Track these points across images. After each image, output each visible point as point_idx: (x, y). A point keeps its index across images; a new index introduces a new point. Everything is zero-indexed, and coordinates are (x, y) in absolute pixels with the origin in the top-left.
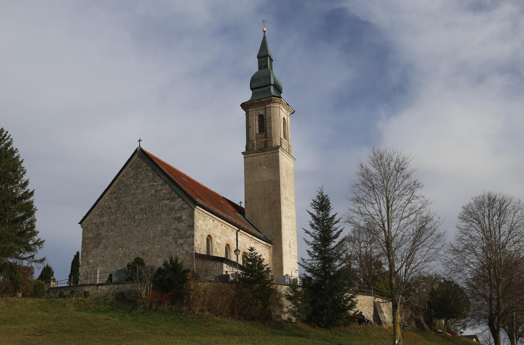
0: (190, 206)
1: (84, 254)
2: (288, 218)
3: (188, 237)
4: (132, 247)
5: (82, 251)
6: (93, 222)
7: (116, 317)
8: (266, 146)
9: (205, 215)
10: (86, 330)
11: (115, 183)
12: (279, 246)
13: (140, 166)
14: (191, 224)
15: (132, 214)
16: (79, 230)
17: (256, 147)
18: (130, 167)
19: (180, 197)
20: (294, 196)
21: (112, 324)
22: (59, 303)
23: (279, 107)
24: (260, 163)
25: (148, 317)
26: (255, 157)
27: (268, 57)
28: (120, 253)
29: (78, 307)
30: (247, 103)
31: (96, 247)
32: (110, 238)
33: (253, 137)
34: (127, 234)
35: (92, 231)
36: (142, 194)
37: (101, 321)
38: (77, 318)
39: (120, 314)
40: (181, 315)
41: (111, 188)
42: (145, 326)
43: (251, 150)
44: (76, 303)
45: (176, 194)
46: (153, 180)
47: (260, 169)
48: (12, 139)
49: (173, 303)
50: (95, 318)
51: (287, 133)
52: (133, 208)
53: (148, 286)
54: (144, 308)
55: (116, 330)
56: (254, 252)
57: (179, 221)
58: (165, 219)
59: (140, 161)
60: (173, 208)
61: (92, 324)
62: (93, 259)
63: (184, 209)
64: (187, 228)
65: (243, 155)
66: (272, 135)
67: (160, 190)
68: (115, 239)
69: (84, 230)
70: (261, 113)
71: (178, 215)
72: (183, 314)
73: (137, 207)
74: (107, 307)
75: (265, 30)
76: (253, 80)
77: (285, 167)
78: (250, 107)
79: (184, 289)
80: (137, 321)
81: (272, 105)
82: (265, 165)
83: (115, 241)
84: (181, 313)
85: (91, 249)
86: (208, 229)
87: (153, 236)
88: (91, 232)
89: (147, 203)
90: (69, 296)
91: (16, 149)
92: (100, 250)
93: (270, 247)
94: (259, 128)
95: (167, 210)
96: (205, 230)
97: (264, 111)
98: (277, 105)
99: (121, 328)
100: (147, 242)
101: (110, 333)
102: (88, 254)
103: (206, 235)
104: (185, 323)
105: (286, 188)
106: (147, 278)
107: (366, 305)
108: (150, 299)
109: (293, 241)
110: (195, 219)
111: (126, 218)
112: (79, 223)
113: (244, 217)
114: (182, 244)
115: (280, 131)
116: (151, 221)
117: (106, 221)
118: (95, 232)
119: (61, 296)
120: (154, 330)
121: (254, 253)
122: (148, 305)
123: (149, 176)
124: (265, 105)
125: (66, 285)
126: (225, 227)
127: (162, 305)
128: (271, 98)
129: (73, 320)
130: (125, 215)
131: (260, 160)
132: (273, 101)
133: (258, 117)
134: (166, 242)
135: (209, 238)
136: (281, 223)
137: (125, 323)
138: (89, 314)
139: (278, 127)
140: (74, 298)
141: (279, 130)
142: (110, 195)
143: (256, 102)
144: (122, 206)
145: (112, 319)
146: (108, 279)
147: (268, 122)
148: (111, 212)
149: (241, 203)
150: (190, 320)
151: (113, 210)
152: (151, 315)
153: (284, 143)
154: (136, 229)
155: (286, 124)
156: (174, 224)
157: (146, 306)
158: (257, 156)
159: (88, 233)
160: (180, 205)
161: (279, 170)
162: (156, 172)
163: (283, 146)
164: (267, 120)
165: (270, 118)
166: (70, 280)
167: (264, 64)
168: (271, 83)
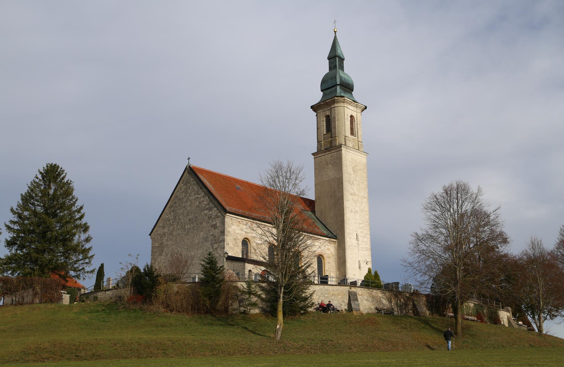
0: (222, 214)
3: (220, 242)
9: (240, 220)
11: (173, 197)
12: (343, 240)
15: (184, 225)
16: (149, 240)
17: (324, 147)
19: (216, 207)
24: (327, 162)
26: (323, 157)
31: (160, 255)
36: (190, 206)
41: (170, 203)
47: (327, 168)
48: (66, 173)
63: (218, 217)
64: (220, 234)
66: (336, 134)
70: (327, 114)
71: (214, 223)
78: (318, 109)
81: (336, 105)
91: (71, 181)
93: (335, 242)
97: (330, 111)
98: (342, 104)
100: (193, 248)
107: (338, 295)
110: (225, 225)
111: (180, 228)
113: (315, 215)
116: (196, 229)
130: (179, 226)
139: (342, 126)
141: (344, 129)
147: (333, 122)
151: (171, 222)
158: (324, 156)
160: (215, 214)
162: (199, 186)
165: (335, 117)
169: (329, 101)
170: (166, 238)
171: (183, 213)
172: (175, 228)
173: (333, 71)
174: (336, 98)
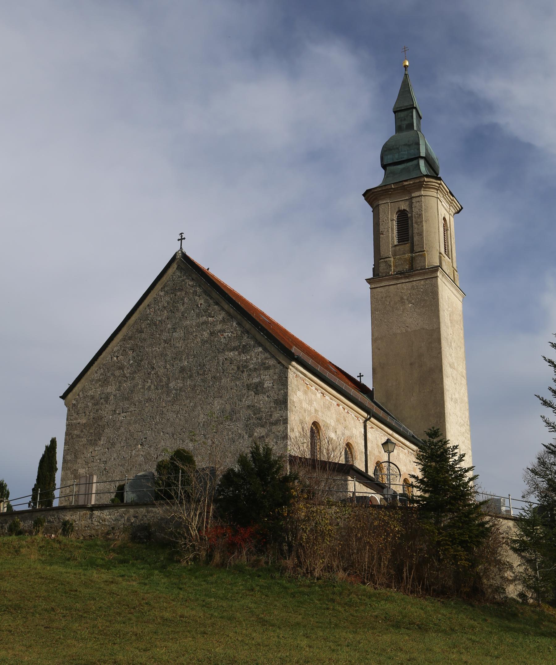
0: (280, 363)
1: (69, 458)
2: (456, 401)
3: (276, 423)
4: (163, 443)
5: (64, 450)
6: (89, 394)
7: (134, 578)
8: (412, 268)
9: (308, 381)
10: (58, 606)
11: (133, 318)
13: (181, 286)
14: (281, 397)
15: (165, 379)
16: (62, 409)
18: (162, 288)
19: (260, 344)
20: (465, 362)
21: (125, 593)
22: (6, 546)
23: (436, 196)
24: (402, 298)
25: (204, 581)
26: (391, 286)
27: (414, 111)
28: (138, 456)
29: (48, 554)
30: (376, 190)
31: (93, 443)
32: (120, 427)
33: (387, 250)
34: (153, 417)
35: (85, 413)
37: (98, 586)
38: (41, 578)
39: (142, 572)
40: (281, 577)
41: (124, 329)
42: (204, 601)
43: (384, 275)
44: (43, 546)
45: (251, 338)
46: (205, 312)
49: (261, 551)
50: (83, 577)
51: (450, 245)
52: (165, 367)
53: (204, 509)
54: (194, 559)
55: (134, 608)
56: (438, 439)
57: (257, 390)
58: (229, 389)
59: (181, 277)
60: (246, 367)
61: (76, 591)
62: (86, 466)
63: (268, 368)
64: (272, 404)
65: (369, 283)
66: (423, 246)
67: (220, 331)
68: (130, 428)
69: (71, 410)
70: (403, 208)
71: (256, 380)
72: (287, 574)
73: (173, 366)
74: (113, 555)
75: (407, 64)
76: (385, 151)
77: (449, 307)
78: (382, 197)
79: (285, 518)
80: (181, 589)
81: (423, 193)
82: (410, 302)
83: (130, 431)
84: (282, 573)
85: (82, 447)
86: (313, 411)
87: (204, 422)
88: (84, 414)
89: (194, 357)
90: (31, 533)
92: (100, 448)
94: (398, 235)
95: (233, 369)
96: (308, 411)
97: (407, 203)
98: (433, 193)
99: (147, 604)
101: (119, 614)
102: (76, 457)
103: (308, 427)
104: (293, 595)
105: (450, 346)
106: (201, 492)
108: (209, 539)
109: (466, 446)
110: (289, 387)
111: (153, 387)
112: (60, 397)
114: (263, 436)
115: (438, 241)
116: (202, 391)
117: (114, 393)
118: (91, 414)
119: (14, 530)
120: (226, 610)
121: (441, 441)
122: (204, 554)
123: (197, 305)
124: (410, 192)
125: (26, 508)
126: (344, 409)
127: (236, 553)
128: (422, 180)
129: (30, 582)
131: (402, 293)
132: (425, 185)
133: (396, 214)
134: (230, 433)
135: (314, 428)
136: (444, 411)
137: (154, 590)
138: (69, 570)
139: (435, 232)
140: (40, 535)
141: (437, 238)
142: (121, 343)
143: (393, 187)
144: (145, 363)
145: (124, 583)
146: (116, 496)
147: (416, 223)
148: (124, 374)
149: (360, 376)
150: (306, 590)
152: (212, 575)
153: (445, 263)
154: (172, 408)
155: (447, 230)
156: (248, 397)
157: (198, 555)
158: (395, 286)
159: (77, 416)
160: (260, 361)
161: (438, 311)
162: (211, 298)
163: (444, 267)
164: (414, 218)
165: (420, 215)
166: (34, 498)
167: (406, 122)
168: (420, 154)
169: (410, 184)
170: (110, 407)
171: (163, 355)
172: (137, 385)
173: (406, 135)
174: (426, 179)
